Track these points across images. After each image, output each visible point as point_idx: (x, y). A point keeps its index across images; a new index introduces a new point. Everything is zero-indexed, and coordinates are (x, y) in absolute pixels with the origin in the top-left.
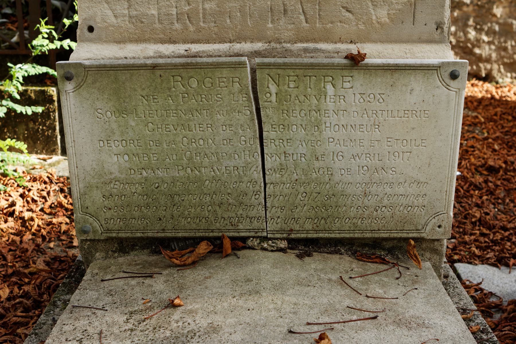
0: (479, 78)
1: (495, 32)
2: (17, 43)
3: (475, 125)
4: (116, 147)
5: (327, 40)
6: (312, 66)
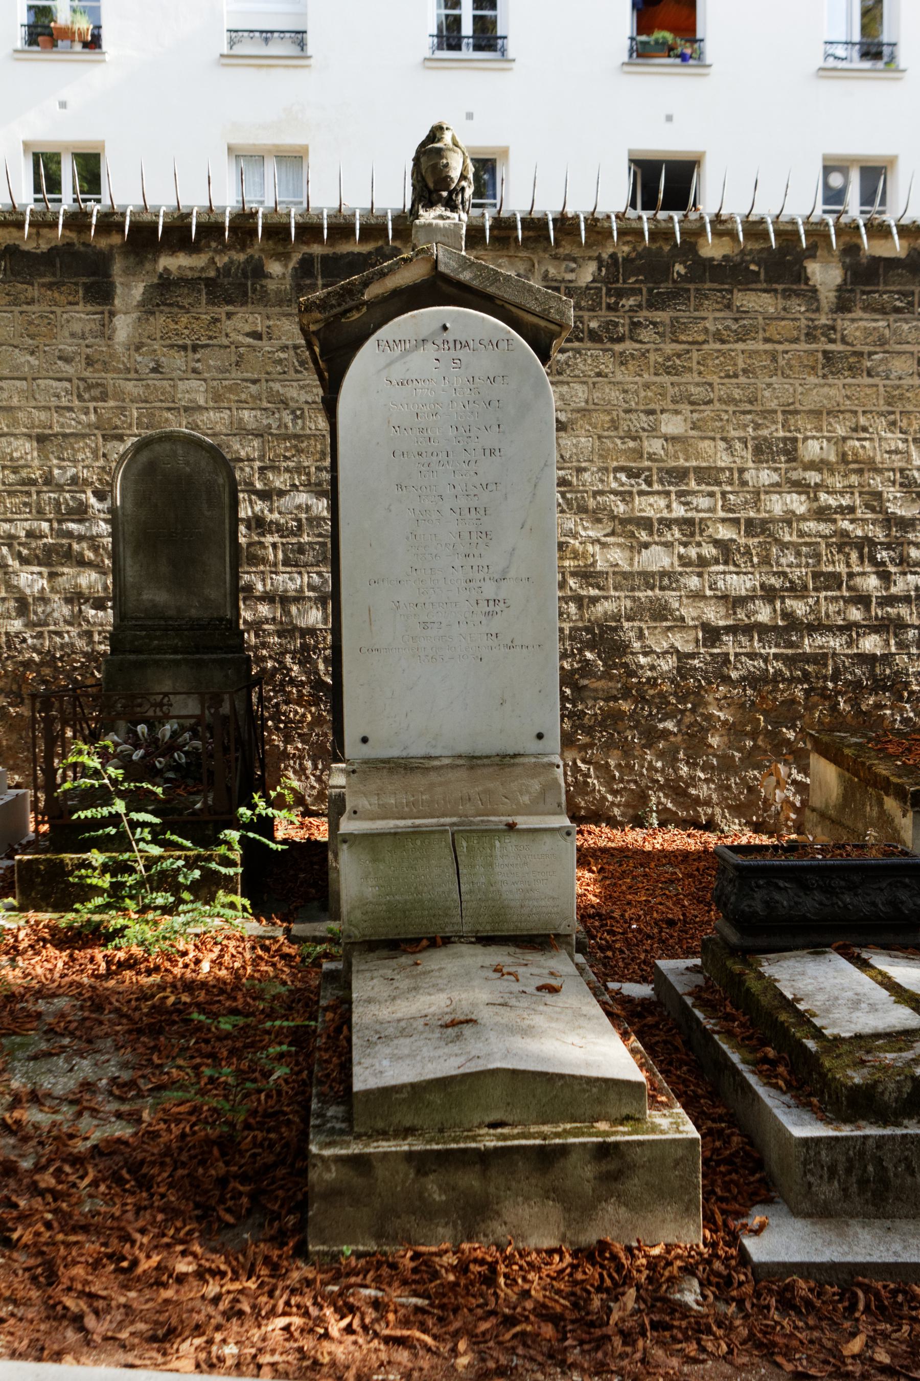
0: (698, 826)
1: (713, 767)
2: (201, 809)
3: (672, 882)
4: (371, 882)
5: (494, 815)
6: (486, 831)
